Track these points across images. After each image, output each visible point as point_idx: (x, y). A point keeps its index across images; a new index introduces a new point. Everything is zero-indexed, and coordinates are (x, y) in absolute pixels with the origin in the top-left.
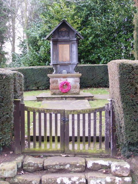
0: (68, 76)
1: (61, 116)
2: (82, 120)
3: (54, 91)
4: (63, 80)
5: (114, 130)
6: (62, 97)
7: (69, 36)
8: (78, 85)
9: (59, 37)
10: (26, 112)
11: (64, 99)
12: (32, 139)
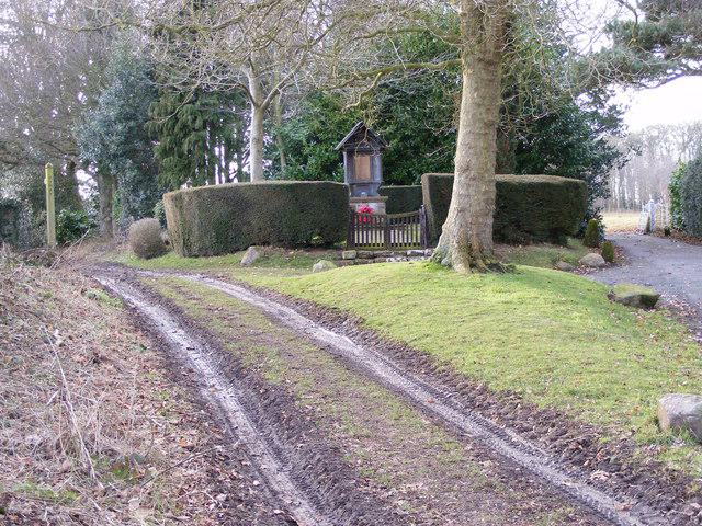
4: (363, 206)
5: (427, 230)
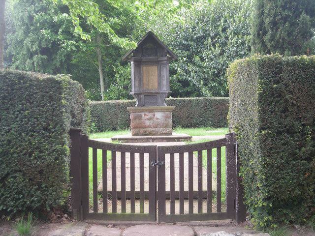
0: (154, 109)
1: (228, 150)
2: (194, 166)
3: (137, 130)
6: (147, 139)
7: (156, 55)
8: (170, 122)
9: (143, 55)
10: (91, 150)
11: (151, 141)
12: (105, 194)
